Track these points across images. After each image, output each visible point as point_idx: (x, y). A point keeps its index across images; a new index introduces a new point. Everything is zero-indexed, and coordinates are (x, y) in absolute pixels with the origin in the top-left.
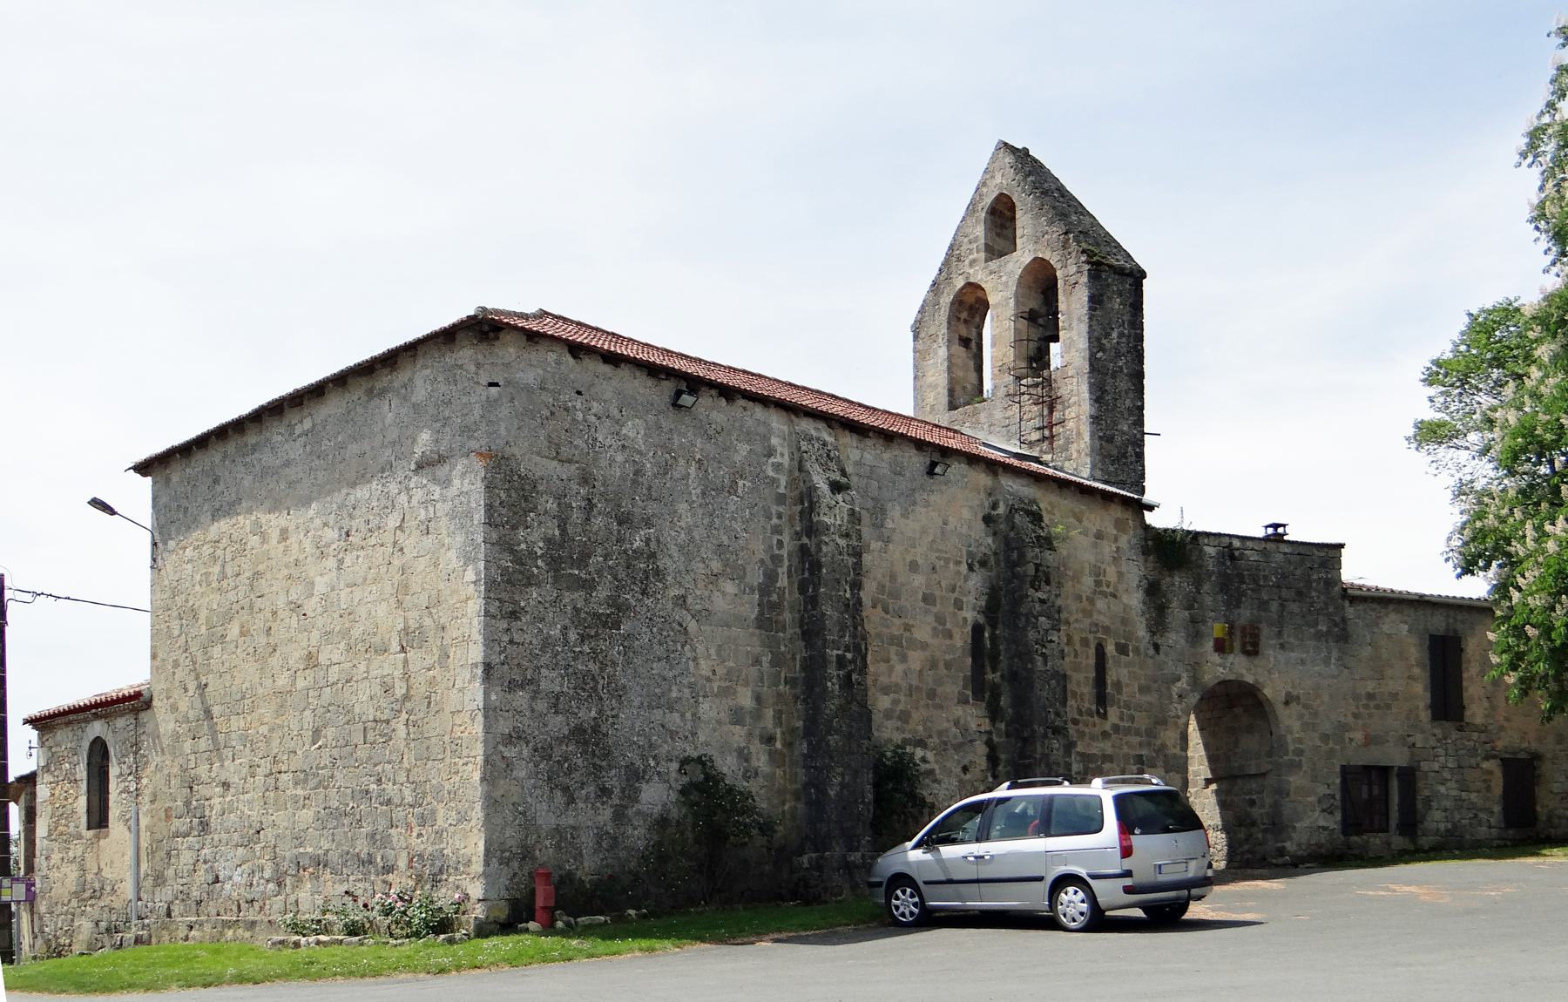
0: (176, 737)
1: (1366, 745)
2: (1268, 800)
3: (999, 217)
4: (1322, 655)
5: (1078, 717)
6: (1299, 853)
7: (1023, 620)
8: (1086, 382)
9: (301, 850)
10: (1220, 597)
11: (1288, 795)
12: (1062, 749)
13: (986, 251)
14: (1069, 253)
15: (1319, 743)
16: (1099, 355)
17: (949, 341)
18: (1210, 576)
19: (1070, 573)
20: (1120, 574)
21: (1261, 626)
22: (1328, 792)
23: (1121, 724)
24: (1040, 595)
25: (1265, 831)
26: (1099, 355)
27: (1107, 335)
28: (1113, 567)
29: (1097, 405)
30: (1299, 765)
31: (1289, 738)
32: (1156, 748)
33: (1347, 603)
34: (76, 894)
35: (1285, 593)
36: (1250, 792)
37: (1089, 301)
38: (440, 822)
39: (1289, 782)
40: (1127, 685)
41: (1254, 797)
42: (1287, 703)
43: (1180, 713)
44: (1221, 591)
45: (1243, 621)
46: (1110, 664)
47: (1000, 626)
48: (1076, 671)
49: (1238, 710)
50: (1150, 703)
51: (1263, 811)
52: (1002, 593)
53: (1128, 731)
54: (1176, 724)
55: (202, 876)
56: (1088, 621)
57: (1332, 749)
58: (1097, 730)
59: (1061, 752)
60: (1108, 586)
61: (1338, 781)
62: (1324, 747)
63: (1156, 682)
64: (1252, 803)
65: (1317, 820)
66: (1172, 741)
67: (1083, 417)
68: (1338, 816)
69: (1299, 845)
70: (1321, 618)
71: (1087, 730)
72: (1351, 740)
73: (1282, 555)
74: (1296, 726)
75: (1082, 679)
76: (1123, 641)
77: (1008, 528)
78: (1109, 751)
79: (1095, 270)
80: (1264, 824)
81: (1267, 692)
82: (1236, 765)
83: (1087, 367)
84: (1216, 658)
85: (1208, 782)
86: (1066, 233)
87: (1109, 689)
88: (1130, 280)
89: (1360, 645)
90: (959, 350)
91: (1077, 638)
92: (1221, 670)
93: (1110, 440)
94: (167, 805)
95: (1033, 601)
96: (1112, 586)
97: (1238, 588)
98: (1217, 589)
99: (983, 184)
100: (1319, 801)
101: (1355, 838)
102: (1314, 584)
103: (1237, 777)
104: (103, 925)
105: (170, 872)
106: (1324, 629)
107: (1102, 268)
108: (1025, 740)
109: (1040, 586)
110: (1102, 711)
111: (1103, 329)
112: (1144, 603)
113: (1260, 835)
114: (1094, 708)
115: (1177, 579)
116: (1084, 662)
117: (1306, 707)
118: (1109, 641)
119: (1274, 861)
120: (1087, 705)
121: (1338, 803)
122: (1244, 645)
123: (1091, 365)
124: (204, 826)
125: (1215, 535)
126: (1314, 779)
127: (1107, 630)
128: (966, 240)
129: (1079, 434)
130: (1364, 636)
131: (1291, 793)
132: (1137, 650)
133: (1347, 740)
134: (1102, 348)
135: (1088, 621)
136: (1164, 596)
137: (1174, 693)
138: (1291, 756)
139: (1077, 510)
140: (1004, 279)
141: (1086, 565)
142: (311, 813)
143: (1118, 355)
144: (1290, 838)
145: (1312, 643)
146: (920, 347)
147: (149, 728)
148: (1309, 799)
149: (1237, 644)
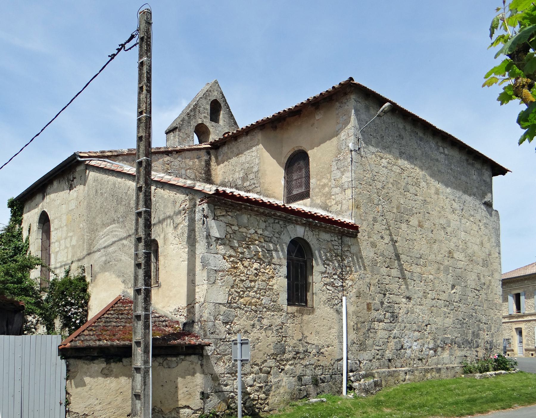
0: (374, 263)
9: (446, 336)
34: (274, 356)
38: (492, 331)
55: (392, 344)
94: (368, 301)
104: (307, 378)
105: (369, 342)
124: (394, 317)
142: (451, 320)
147: (354, 249)
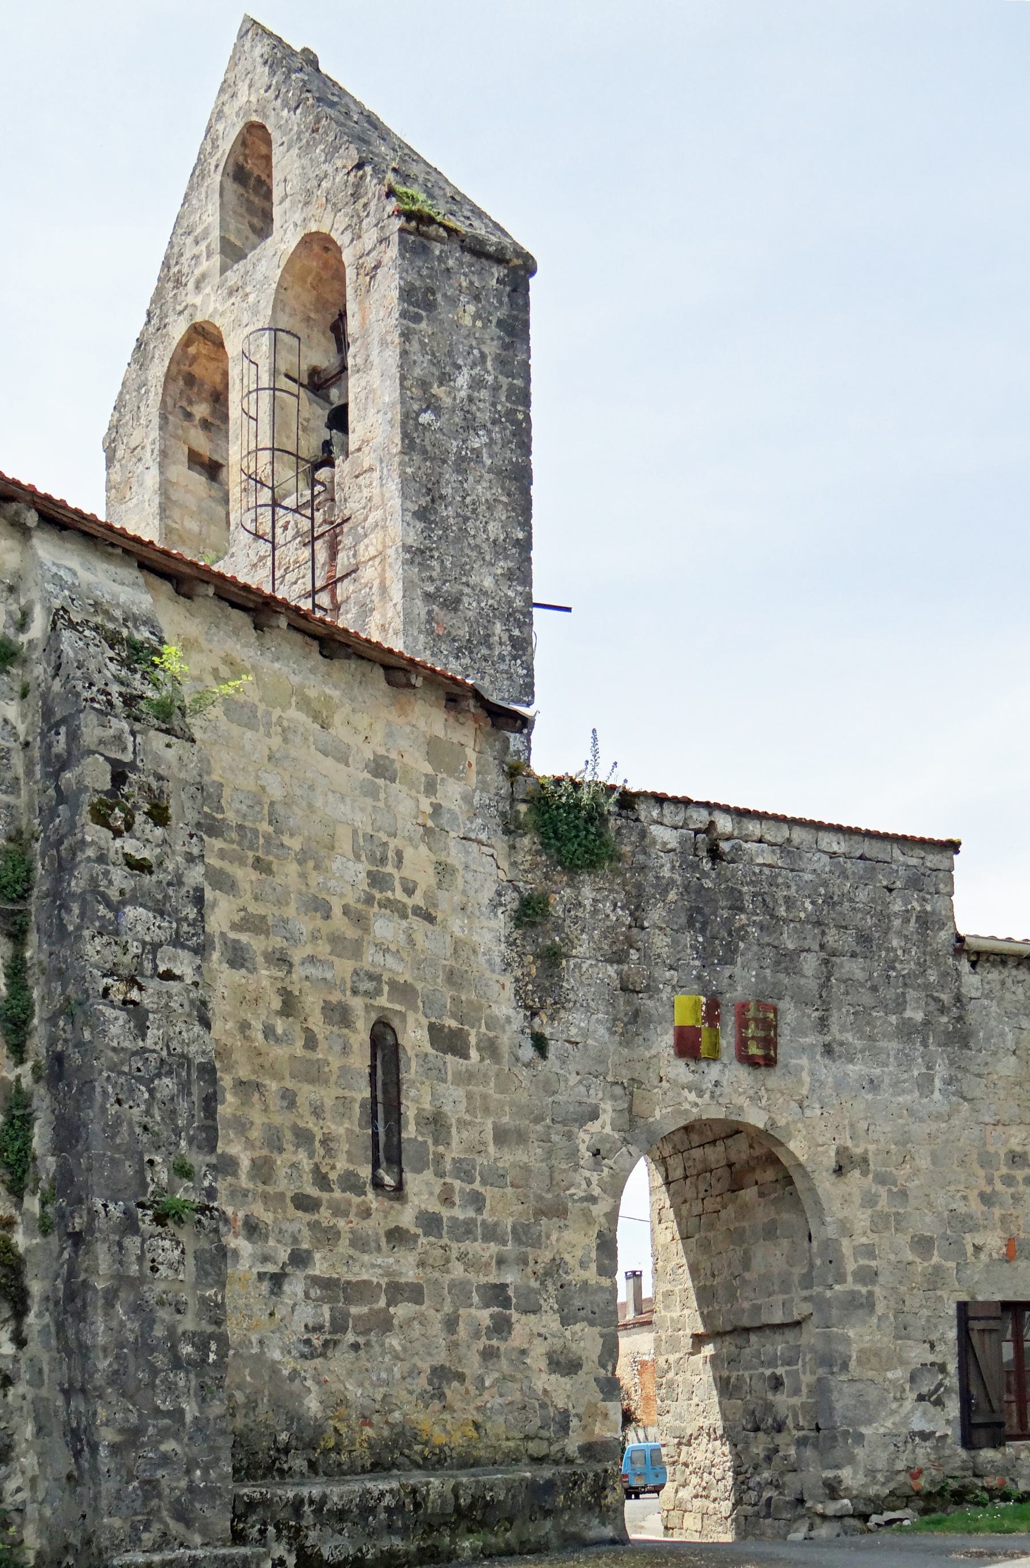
1: (1010, 1257)
2: (807, 1379)
3: (256, 191)
4: (916, 1073)
5: (313, 1191)
6: (872, 1491)
7: (76, 909)
8: (395, 475)
10: (687, 938)
11: (845, 1366)
12: (190, 1261)
13: (223, 252)
14: (365, 205)
15: (910, 1256)
16: (426, 418)
17: (164, 453)
18: (665, 892)
19: (295, 844)
20: (443, 870)
21: (782, 1005)
22: (931, 1358)
23: (446, 1213)
24: (130, 845)
25: (802, 1442)
26: (426, 418)
27: (444, 379)
28: (423, 849)
29: (420, 525)
30: (869, 1304)
31: (846, 1247)
32: (540, 1268)
33: (965, 966)
35: (832, 937)
36: (772, 1363)
37: (401, 298)
39: (847, 1340)
40: (462, 1124)
41: (780, 1371)
42: (839, 1171)
43: (597, 1191)
44: (691, 923)
45: (738, 993)
46: (411, 1072)
47: (33, 937)
48: (312, 1081)
49: (749, 1194)
50: (526, 1169)
51: (796, 1401)
52: (37, 846)
53: (465, 1230)
54: (588, 1218)
56: (345, 968)
57: (937, 1269)
58: (375, 1226)
59: (188, 1272)
60: (410, 891)
61: (952, 1334)
62: (921, 1266)
63: (538, 1119)
64: (777, 1383)
65: (906, 1420)
66: (579, 1253)
67: (391, 552)
68: (953, 1408)
69: (871, 1473)
70: (911, 994)
71: (341, 1223)
72: (978, 1249)
73: (825, 859)
74: (861, 1219)
75: (329, 1103)
76: (454, 1024)
77: (50, 671)
78: (410, 1274)
79: (417, 232)
80: (802, 1429)
81: (797, 1147)
82: (746, 1305)
83: (398, 440)
84: (679, 1070)
85: (699, 1340)
86: (359, 166)
87: (410, 1131)
88: (498, 272)
89: (994, 1054)
90: (181, 472)
91: (312, 1002)
92: (692, 1097)
93: (453, 604)
95: (102, 859)
96: (419, 893)
97: (728, 922)
98: (683, 920)
99: (219, 114)
100: (913, 1379)
101: (987, 1454)
102: (897, 923)
103: (747, 1330)
106: (919, 1016)
107: (432, 230)
108: (77, 1239)
109: (129, 826)
110: (389, 1180)
111: (435, 363)
112: (512, 944)
113: (792, 1451)
114: (365, 1172)
115: (588, 893)
116: (335, 1063)
117: (882, 1179)
118: (411, 1017)
119: (819, 1508)
120: (342, 1164)
121: (953, 1381)
122: (743, 1043)
123: (405, 435)
125: (675, 801)
126: (902, 1331)
127: (403, 991)
128: (190, 240)
129: (384, 589)
130: (1002, 1035)
131: (853, 1364)
132: (490, 1048)
133: (970, 1250)
134: (432, 405)
135: (345, 968)
136: (558, 928)
137: (583, 1148)
138: (850, 1284)
139: (312, 693)
140: (251, 298)
141: (344, 836)
143: (470, 425)
144: (851, 1460)
145: (893, 1045)
146: (116, 478)
148: (890, 1375)
149: (728, 1042)
